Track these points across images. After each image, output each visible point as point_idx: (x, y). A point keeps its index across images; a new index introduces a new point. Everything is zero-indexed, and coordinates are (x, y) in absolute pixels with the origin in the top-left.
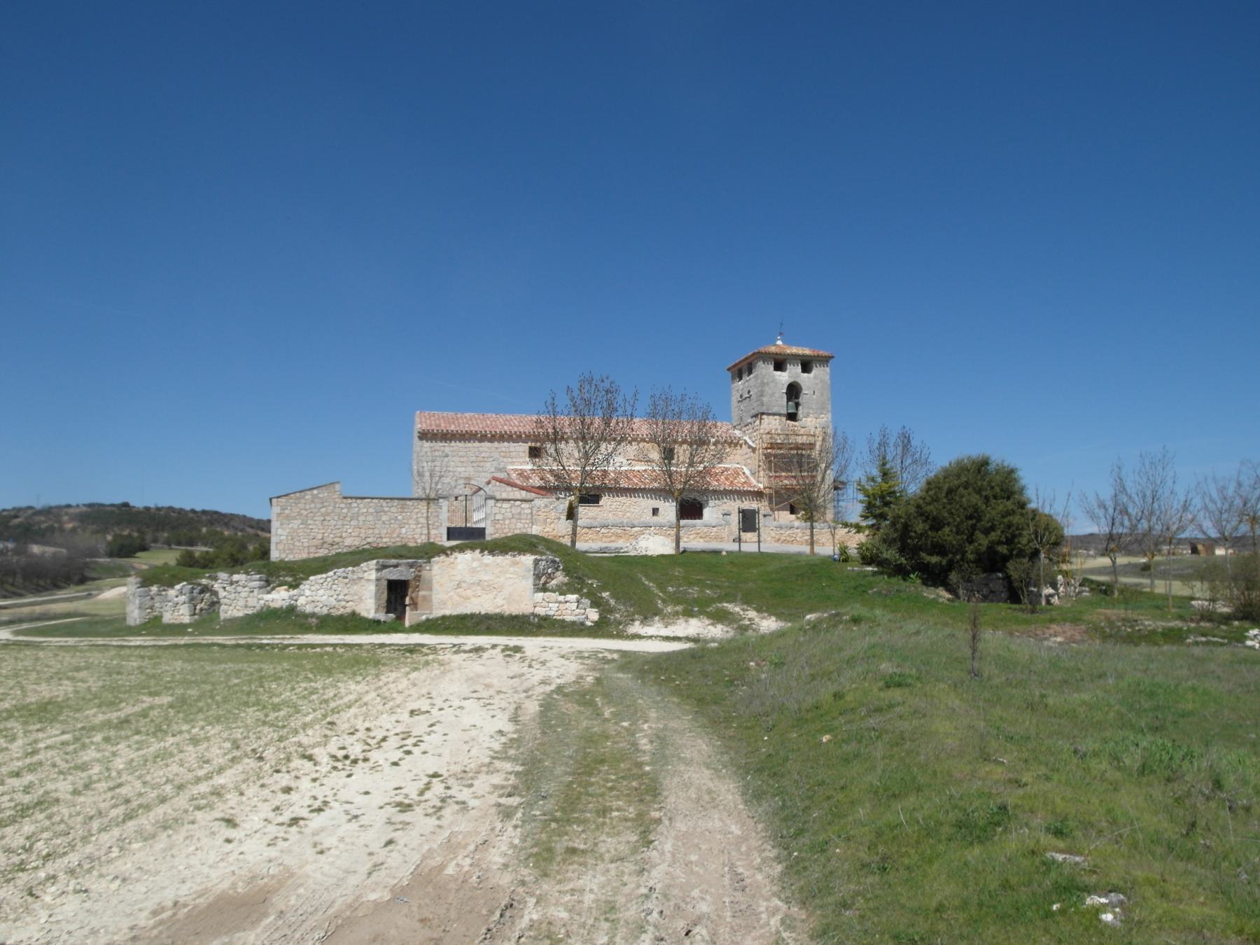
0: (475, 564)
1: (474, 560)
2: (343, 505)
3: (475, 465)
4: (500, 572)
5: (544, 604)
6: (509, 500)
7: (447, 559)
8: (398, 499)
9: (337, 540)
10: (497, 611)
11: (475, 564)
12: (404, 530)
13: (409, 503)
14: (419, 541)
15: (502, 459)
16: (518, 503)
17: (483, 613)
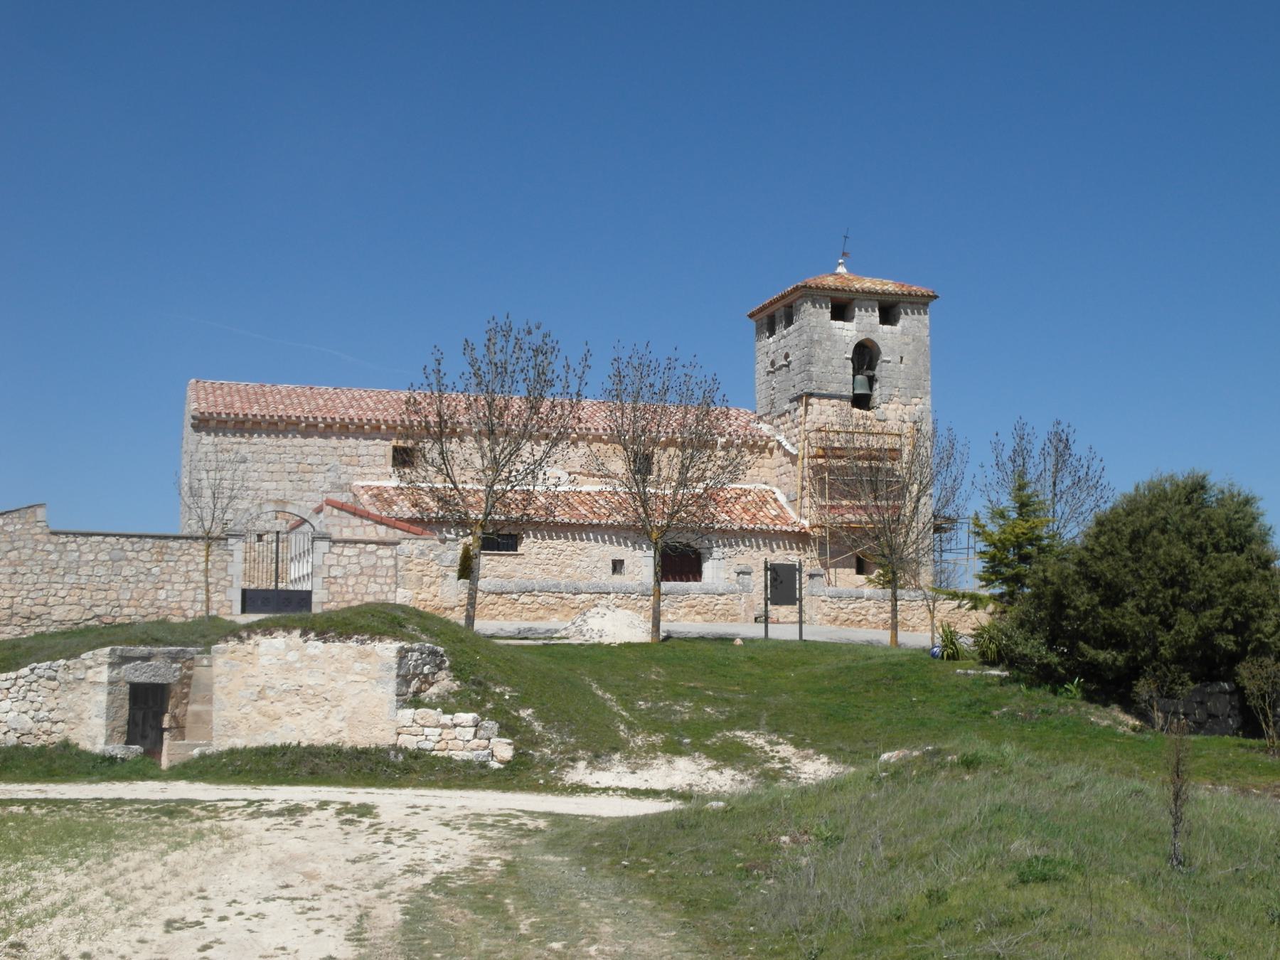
0: (292, 656)
1: (289, 648)
2: (50, 547)
3: (294, 477)
4: (337, 670)
5: (416, 729)
6: (356, 542)
7: (240, 646)
8: (152, 537)
9: (37, 609)
10: (331, 741)
11: (292, 656)
15: (344, 468)
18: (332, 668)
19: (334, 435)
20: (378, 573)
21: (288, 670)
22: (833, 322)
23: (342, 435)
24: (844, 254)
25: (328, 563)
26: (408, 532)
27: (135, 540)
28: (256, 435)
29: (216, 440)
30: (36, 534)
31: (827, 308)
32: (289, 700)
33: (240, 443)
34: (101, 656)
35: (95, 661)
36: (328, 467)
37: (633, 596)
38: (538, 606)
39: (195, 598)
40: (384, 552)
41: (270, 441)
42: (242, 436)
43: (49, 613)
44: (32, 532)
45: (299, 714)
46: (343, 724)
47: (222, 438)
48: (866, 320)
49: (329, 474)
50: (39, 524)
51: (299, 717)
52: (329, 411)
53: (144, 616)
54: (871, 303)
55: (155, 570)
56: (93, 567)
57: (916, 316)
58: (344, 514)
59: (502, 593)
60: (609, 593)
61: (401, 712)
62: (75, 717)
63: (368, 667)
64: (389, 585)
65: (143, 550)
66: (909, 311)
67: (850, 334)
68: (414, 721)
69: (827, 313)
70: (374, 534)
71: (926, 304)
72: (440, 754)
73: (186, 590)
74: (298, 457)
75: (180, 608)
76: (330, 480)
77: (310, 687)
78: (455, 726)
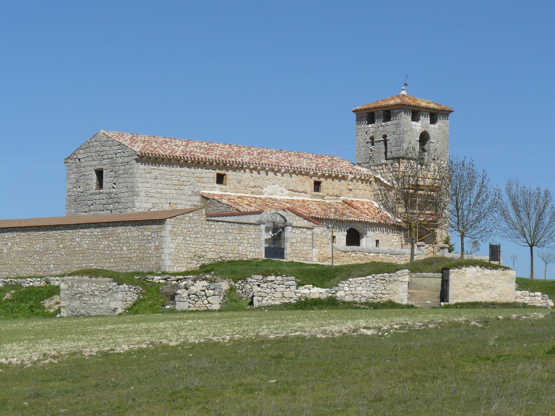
0: (479, 274)
1: (478, 272)
2: (206, 226)
3: (177, 187)
4: (495, 279)
5: (522, 297)
6: (300, 227)
7: (460, 271)
8: (237, 223)
9: (203, 253)
10: (492, 300)
11: (479, 274)
12: (240, 248)
13: (244, 226)
14: (249, 257)
15: (196, 184)
16: (304, 230)
17: (483, 301)
18: (493, 278)
19: (193, 167)
20: (307, 242)
21: (477, 278)
22: (412, 122)
23: (196, 167)
24: (406, 85)
25: (291, 237)
26: (315, 223)
27: (232, 224)
28: (161, 165)
29: (145, 167)
30: (202, 221)
31: (410, 115)
32: (477, 288)
33: (154, 169)
34: (405, 272)
35: (402, 274)
36: (190, 183)
37: (387, 255)
38: (357, 258)
39: (251, 250)
40: (309, 232)
41: (167, 168)
42: (156, 165)
43: (206, 255)
44: (201, 219)
45: (481, 292)
46: (497, 295)
47: (147, 166)
48: (424, 122)
49: (191, 186)
50: (203, 216)
51: (481, 293)
52: (232, 157)
53: (235, 258)
54: (426, 113)
55: (238, 238)
56: (219, 235)
57: (444, 121)
58: (294, 214)
59: (346, 252)
60: (380, 253)
61: (517, 292)
62: (393, 293)
63: (506, 278)
64: (310, 247)
65: (235, 229)
66: (426, 116)
67: (418, 128)
68: (521, 295)
69: (410, 118)
70: (303, 224)
71: (448, 115)
72: (531, 304)
73: (248, 247)
74: (178, 177)
75: (246, 254)
76: (191, 189)
77: (485, 284)
78: (535, 296)
